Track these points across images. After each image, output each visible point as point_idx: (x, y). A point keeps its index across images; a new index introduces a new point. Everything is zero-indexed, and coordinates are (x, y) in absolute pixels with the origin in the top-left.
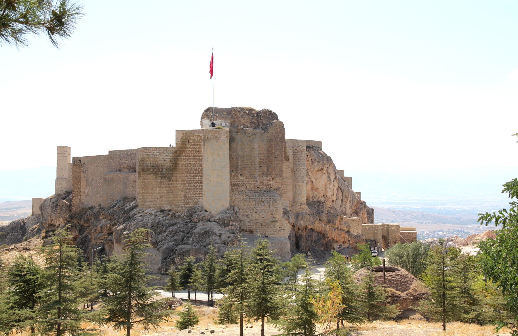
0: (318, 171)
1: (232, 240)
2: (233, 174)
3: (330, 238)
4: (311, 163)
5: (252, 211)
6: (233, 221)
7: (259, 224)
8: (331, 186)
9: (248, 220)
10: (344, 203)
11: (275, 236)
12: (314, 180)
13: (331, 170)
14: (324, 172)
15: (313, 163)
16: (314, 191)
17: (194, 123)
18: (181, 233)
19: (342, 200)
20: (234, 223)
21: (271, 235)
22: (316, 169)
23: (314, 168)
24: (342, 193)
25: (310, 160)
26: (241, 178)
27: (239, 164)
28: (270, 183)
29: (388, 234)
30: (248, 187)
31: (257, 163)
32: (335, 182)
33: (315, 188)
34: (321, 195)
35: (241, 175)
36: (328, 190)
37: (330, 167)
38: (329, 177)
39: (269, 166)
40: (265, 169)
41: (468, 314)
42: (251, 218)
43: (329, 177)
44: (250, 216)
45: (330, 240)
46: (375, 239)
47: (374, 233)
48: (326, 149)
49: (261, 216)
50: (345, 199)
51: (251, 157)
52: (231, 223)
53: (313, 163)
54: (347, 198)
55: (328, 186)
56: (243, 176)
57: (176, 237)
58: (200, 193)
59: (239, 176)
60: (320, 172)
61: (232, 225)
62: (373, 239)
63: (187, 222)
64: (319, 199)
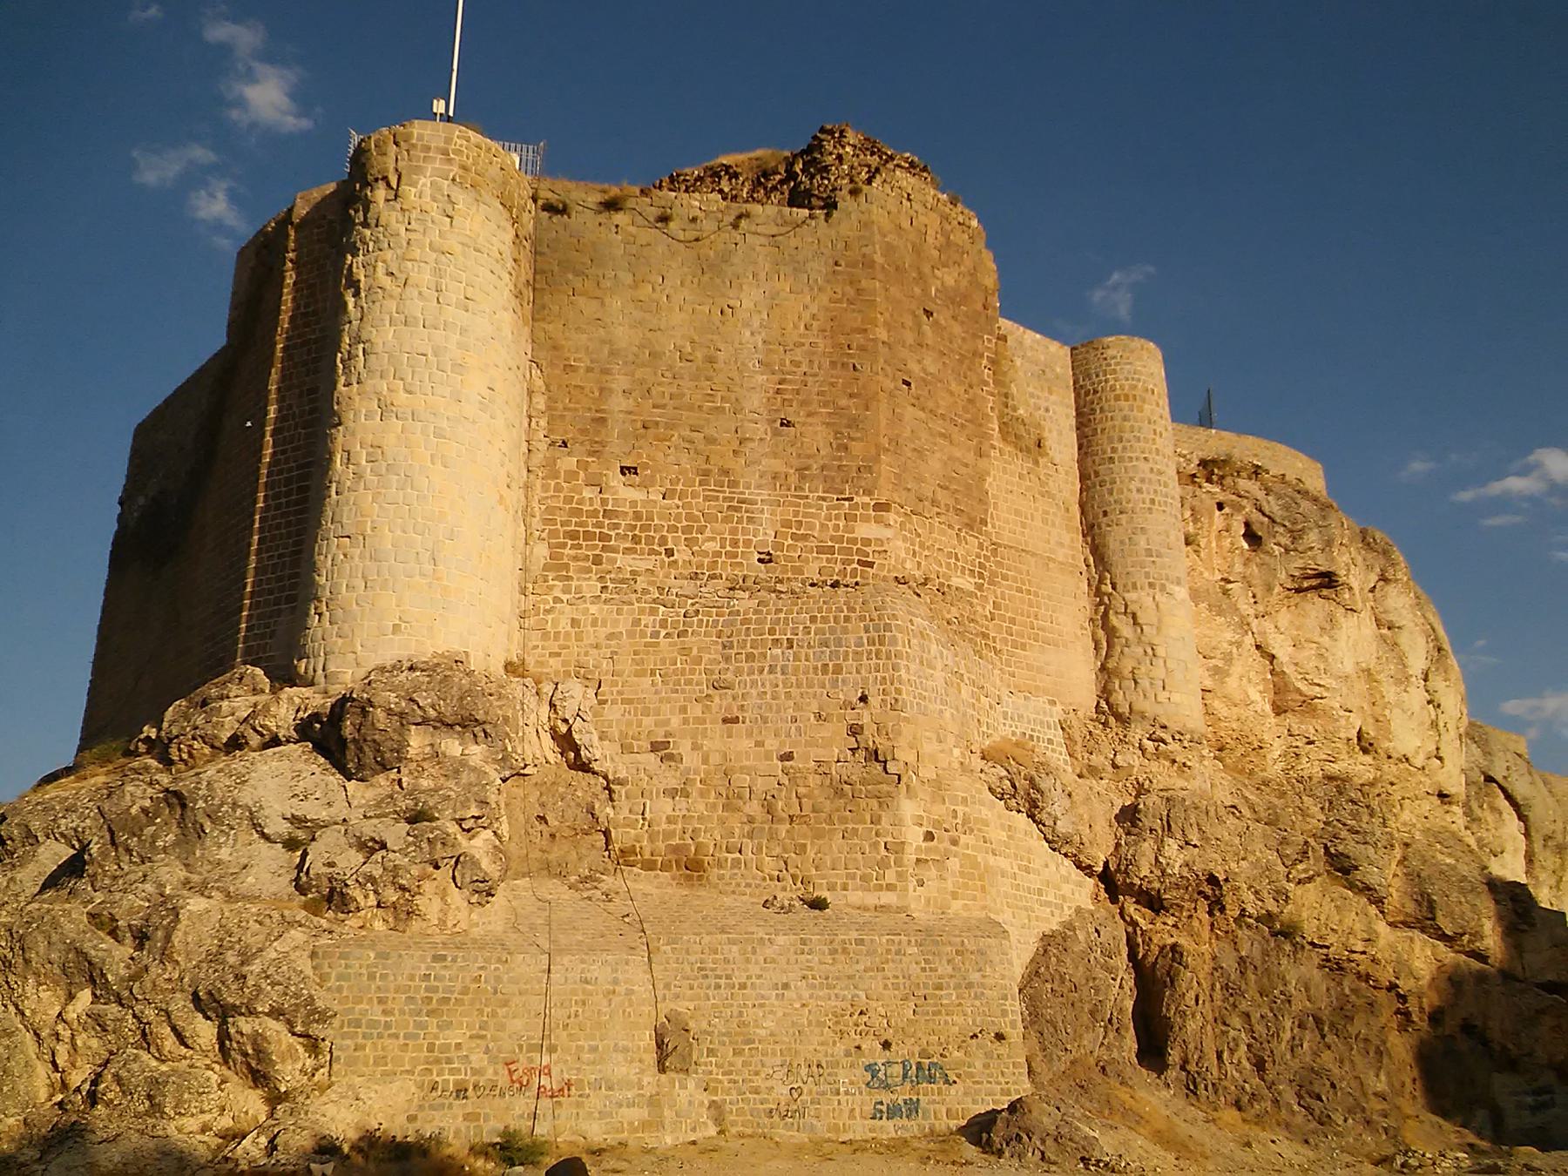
5: (696, 710)
7: (754, 808)
11: (888, 898)
21: (856, 897)
26: (624, 492)
27: (618, 404)
28: (864, 530)
30: (682, 555)
31: (755, 401)
32: (1437, 682)
39: (846, 427)
40: (816, 436)
42: (690, 760)
44: (683, 747)
49: (772, 744)
59: (616, 480)
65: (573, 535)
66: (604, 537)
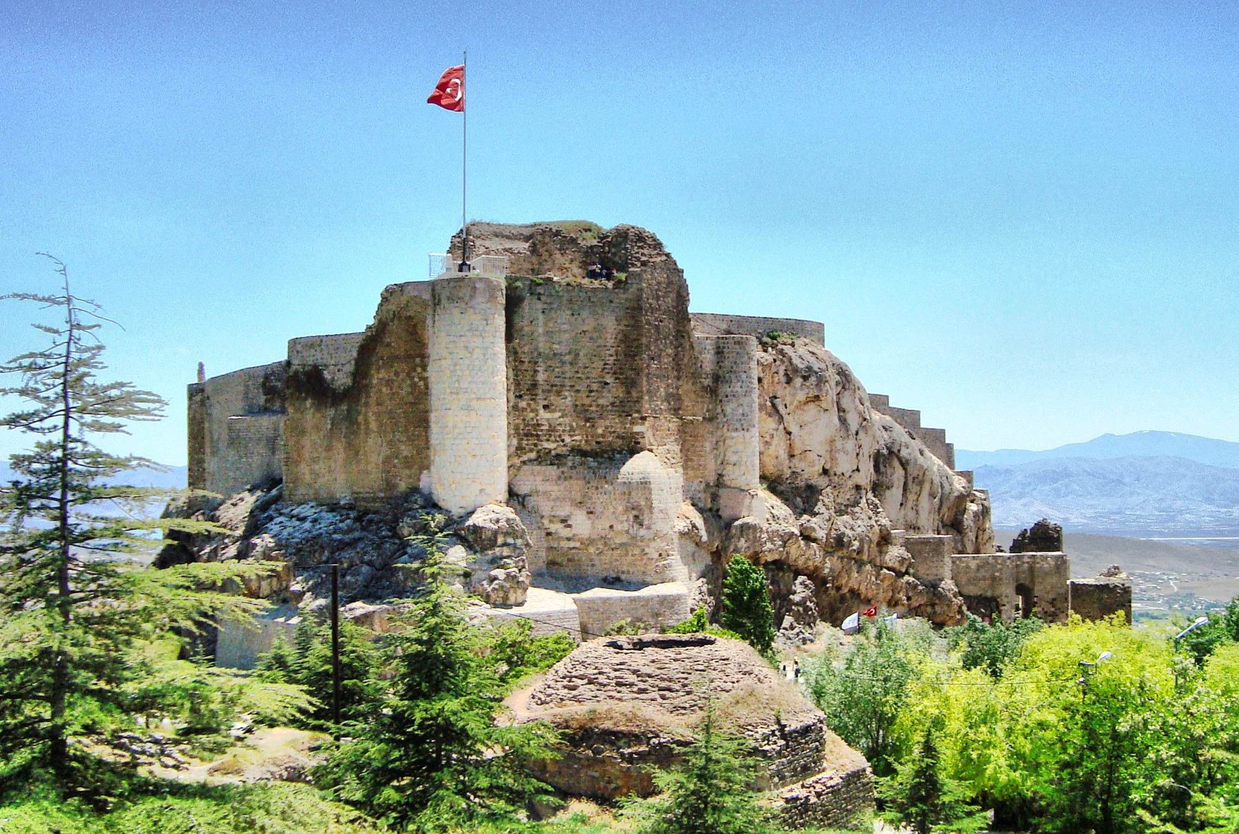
0: (806, 403)
1: (502, 587)
2: (523, 404)
3: (845, 590)
4: (783, 379)
6: (506, 534)
8: (850, 445)
9: (565, 532)
10: (911, 497)
12: (793, 428)
13: (846, 402)
14: (824, 405)
15: (789, 381)
16: (795, 461)
17: (425, 262)
18: (365, 569)
19: (905, 489)
20: (510, 540)
22: (801, 396)
23: (794, 395)
24: (905, 469)
25: (782, 373)
26: (544, 415)
27: (541, 377)
28: (637, 429)
29: (1032, 581)
32: (861, 434)
33: (796, 452)
34: (819, 468)
35: (545, 407)
36: (841, 457)
37: (847, 393)
38: (843, 421)
41: (45, 652)
43: (843, 421)
45: (843, 598)
46: (997, 593)
47: (994, 579)
48: (839, 346)
50: (913, 488)
51: (578, 355)
52: (500, 540)
53: (789, 381)
54: (921, 483)
55: (839, 444)
56: (554, 411)
57: (348, 578)
58: (421, 460)
59: (542, 411)
60: (812, 405)
61: (505, 544)
62: (989, 594)
63: (384, 537)
64: (812, 482)
65: (526, 435)
66: (538, 435)
